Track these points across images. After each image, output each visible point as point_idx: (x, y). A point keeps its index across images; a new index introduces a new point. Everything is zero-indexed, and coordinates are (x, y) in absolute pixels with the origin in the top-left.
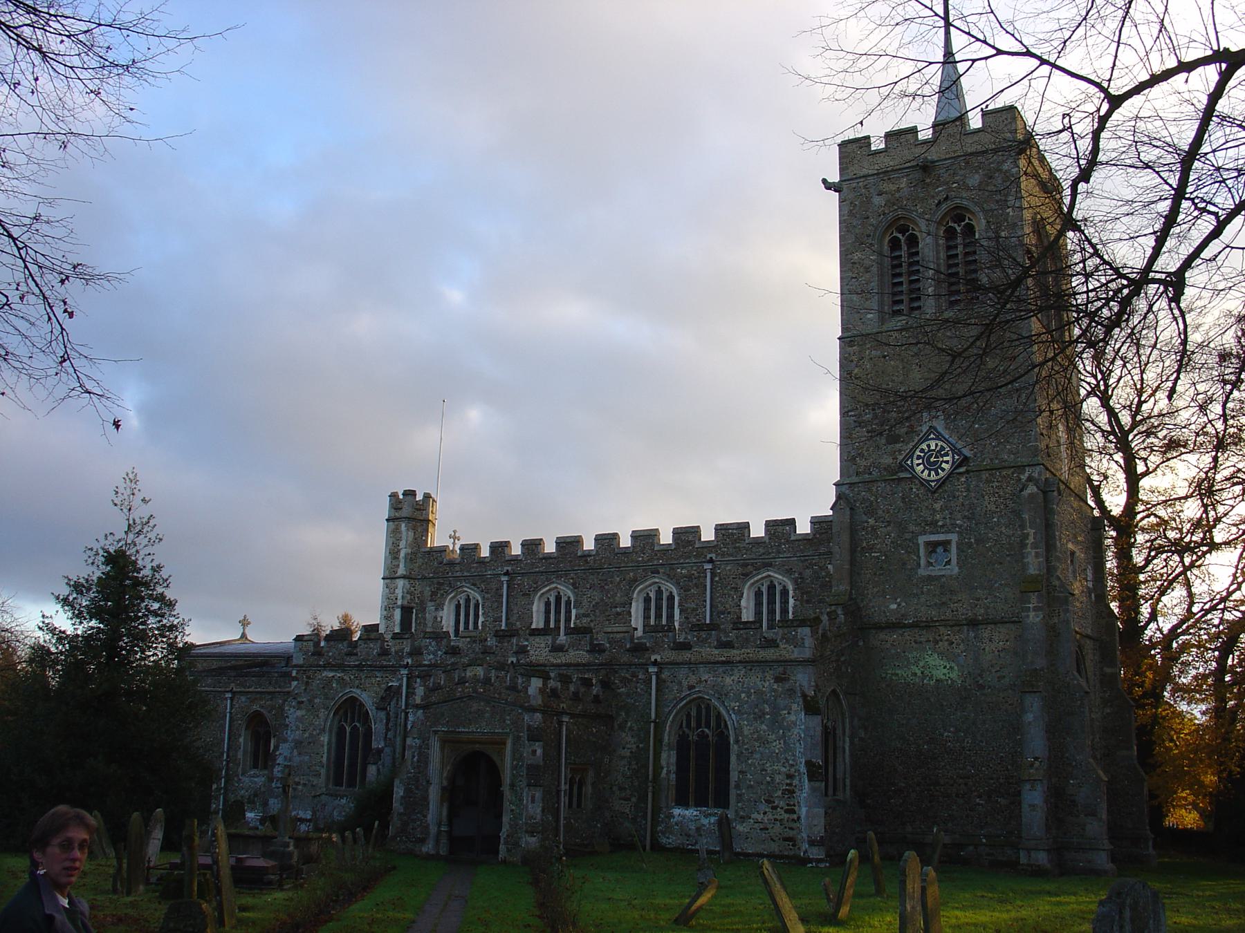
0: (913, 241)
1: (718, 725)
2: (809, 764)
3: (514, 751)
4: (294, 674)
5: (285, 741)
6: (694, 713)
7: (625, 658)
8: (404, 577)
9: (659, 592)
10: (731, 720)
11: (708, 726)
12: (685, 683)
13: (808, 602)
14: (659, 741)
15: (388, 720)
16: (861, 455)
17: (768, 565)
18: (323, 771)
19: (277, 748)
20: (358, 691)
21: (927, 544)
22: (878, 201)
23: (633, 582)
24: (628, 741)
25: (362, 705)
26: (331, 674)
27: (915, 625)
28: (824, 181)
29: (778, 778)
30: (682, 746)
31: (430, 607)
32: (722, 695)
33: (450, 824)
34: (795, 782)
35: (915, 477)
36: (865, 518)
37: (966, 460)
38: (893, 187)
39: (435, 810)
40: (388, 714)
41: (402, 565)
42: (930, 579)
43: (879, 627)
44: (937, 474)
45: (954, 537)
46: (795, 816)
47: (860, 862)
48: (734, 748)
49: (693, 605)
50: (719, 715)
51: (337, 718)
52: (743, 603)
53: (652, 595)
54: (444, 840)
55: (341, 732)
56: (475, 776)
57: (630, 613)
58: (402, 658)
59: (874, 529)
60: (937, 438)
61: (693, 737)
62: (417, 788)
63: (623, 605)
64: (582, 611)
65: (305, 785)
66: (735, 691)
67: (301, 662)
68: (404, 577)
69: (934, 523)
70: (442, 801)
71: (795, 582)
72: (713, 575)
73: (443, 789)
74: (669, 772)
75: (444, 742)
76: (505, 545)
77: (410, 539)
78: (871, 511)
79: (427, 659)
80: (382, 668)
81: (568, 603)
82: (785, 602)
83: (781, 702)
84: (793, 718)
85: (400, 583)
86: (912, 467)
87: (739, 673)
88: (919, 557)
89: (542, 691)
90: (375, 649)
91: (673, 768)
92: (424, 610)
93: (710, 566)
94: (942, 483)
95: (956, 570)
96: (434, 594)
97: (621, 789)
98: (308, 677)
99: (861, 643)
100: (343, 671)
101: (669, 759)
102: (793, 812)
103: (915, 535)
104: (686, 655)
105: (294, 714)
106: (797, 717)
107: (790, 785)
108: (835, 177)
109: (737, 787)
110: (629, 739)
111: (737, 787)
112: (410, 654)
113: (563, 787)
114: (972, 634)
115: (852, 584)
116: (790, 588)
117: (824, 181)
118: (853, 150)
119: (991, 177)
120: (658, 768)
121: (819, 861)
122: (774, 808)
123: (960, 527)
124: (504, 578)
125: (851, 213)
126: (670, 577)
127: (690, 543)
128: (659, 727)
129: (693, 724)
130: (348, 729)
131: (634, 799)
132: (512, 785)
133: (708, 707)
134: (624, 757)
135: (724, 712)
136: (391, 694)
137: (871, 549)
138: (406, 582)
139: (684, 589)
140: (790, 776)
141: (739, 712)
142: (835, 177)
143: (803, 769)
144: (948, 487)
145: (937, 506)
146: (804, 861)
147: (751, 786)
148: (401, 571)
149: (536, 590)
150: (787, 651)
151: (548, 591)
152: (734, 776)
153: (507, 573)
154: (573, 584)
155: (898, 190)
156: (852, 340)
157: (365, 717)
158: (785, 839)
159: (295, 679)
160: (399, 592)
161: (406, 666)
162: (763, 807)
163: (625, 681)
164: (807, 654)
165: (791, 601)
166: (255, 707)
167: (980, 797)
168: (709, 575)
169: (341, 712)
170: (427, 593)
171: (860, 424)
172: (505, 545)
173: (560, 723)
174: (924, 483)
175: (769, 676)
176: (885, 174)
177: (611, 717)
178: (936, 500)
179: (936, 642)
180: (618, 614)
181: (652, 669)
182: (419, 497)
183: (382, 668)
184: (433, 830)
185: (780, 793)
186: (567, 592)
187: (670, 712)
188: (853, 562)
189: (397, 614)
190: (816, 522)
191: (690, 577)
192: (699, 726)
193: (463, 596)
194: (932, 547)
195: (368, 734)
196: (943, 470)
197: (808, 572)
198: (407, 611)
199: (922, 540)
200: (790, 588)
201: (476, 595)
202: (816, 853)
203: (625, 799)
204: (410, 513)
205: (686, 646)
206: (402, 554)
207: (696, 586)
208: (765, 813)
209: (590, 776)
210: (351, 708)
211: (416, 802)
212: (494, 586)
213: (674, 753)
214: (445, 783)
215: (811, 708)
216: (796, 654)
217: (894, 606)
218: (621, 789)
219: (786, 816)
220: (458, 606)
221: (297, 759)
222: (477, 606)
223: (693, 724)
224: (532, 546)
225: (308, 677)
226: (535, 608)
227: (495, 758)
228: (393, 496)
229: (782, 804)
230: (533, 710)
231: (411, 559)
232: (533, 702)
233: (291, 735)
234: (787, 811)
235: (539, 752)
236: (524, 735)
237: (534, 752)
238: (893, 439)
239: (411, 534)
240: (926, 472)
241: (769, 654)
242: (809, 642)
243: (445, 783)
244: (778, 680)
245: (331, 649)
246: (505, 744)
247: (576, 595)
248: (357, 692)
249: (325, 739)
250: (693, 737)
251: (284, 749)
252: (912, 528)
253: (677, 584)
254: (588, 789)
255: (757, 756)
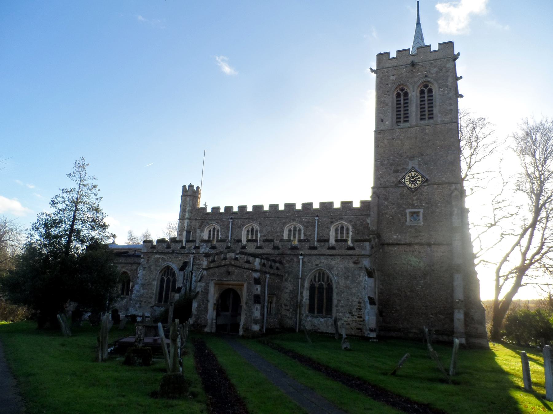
0: (406, 94)
1: (328, 281)
2: (370, 298)
3: (248, 289)
4: (142, 256)
5: (137, 284)
6: (317, 275)
7: (289, 252)
8: (187, 219)
9: (295, 228)
10: (335, 279)
11: (323, 281)
12: (314, 263)
13: (358, 234)
14: (303, 286)
15: (184, 276)
16: (382, 177)
17: (342, 219)
18: (154, 297)
19: (133, 286)
20: (171, 263)
21: (411, 213)
22: (392, 78)
23: (285, 224)
24: (289, 286)
25: (172, 269)
26: (159, 256)
27: (404, 244)
28: (371, 69)
29: (354, 303)
30: (312, 289)
31: (198, 231)
32: (330, 268)
33: (216, 319)
34: (362, 305)
35: (406, 186)
36: (384, 201)
37: (427, 180)
38: (399, 73)
39: (211, 313)
40: (184, 273)
41: (187, 214)
42: (411, 227)
43: (389, 244)
44: (415, 185)
45: (421, 211)
46: (362, 319)
47: (460, 348)
48: (335, 291)
49: (310, 233)
50: (328, 277)
51: (161, 274)
52: (331, 233)
53: (292, 229)
54: (214, 326)
55: (162, 281)
56: (229, 300)
57: (283, 236)
58: (190, 250)
59: (387, 206)
60: (415, 171)
61: (317, 285)
62: (203, 304)
63: (280, 232)
64: (263, 234)
65: (145, 302)
66: (337, 268)
67: (145, 251)
68: (187, 219)
69: (413, 205)
70: (214, 309)
71: (354, 227)
72: (318, 222)
73: (215, 304)
74: (306, 299)
75: (216, 284)
76: (231, 208)
77: (191, 204)
78: (387, 199)
79: (202, 251)
80: (182, 254)
81: (257, 231)
82: (218, 235)
83: (356, 272)
84: (361, 279)
85: (186, 221)
86: (404, 182)
87: (338, 259)
88: (406, 218)
89: (260, 264)
90: (179, 246)
91: (308, 298)
92: (195, 232)
93: (317, 218)
94: (416, 189)
95: (422, 223)
96: (200, 226)
97: (286, 305)
98: (148, 258)
99: (381, 251)
100: (165, 255)
101: (306, 294)
102: (361, 317)
103: (405, 209)
104: (315, 252)
105: (141, 273)
106: (364, 278)
107: (360, 306)
108: (375, 68)
109: (337, 306)
110: (289, 285)
111: (337, 306)
112: (194, 248)
113: (266, 304)
114: (429, 249)
115: (378, 227)
116: (351, 229)
117: (371, 69)
118: (382, 57)
119: (441, 70)
120: (302, 296)
121: (374, 338)
122: (353, 316)
123: (424, 206)
124: (231, 221)
125: (380, 82)
126: (301, 222)
127: (308, 209)
128: (303, 280)
129: (317, 280)
130: (165, 279)
131: (291, 310)
132: (246, 303)
133: (323, 274)
134: (287, 293)
135: (331, 275)
136: (185, 264)
137: (386, 214)
138: (189, 221)
139: (306, 227)
140: (359, 303)
141: (337, 276)
142: (375, 68)
143: (367, 300)
144: (419, 190)
145: (415, 198)
146: (367, 339)
147: (343, 306)
148: (187, 216)
149: (243, 226)
150: (358, 251)
151: (249, 226)
152: (335, 302)
153: (231, 219)
154: (260, 224)
155: (401, 74)
156: (378, 132)
157: (173, 274)
158: (358, 329)
159: (143, 258)
160: (186, 225)
161: (193, 253)
162: (348, 315)
163: (287, 261)
164: (368, 253)
165: (351, 233)
166: (124, 270)
167: (432, 314)
168: (317, 222)
169: (163, 272)
170: (197, 225)
171: (382, 165)
172: (231, 208)
173: (265, 277)
174: (409, 189)
175: (351, 261)
176: (395, 67)
177: (282, 276)
178: (414, 196)
179: (413, 251)
180: (278, 236)
181: (301, 257)
182: (195, 188)
183: (182, 254)
184: (209, 322)
185: (355, 309)
186: (256, 227)
187: (307, 275)
188: (379, 219)
189: (185, 233)
190: (362, 203)
191: (308, 222)
192: (319, 281)
193: (212, 227)
194: (412, 214)
195: (175, 281)
196: (417, 184)
197: (358, 222)
198: (188, 232)
199: (408, 211)
200: (351, 229)
201: (218, 227)
202: (373, 335)
203: (287, 310)
204: (190, 195)
205: (315, 248)
206: (187, 209)
207: (311, 226)
208: (348, 318)
209: (275, 299)
210: (168, 270)
211: (203, 310)
212: (226, 223)
213: (308, 292)
214: (215, 302)
215: (370, 274)
216: (363, 252)
217: (395, 237)
218: (286, 305)
219: (358, 319)
220: (210, 231)
221: (142, 291)
222: (218, 231)
223: (317, 280)
224: (242, 208)
225: (148, 258)
226: (243, 232)
227: (239, 292)
228: (184, 187)
229: (356, 314)
230: (256, 271)
231: (191, 211)
232: (256, 268)
233: (139, 281)
234: (358, 317)
235: (259, 289)
236: (252, 281)
237: (257, 289)
238: (396, 171)
239: (191, 202)
240: (410, 184)
241: (351, 252)
242: (368, 248)
243: (215, 302)
244: (355, 263)
245: (151, 249)
246: (243, 285)
247: (260, 228)
248: (170, 264)
249: (155, 283)
250: (317, 285)
251: (137, 287)
252: (404, 206)
253: (303, 225)
254: (273, 305)
255: (345, 294)
